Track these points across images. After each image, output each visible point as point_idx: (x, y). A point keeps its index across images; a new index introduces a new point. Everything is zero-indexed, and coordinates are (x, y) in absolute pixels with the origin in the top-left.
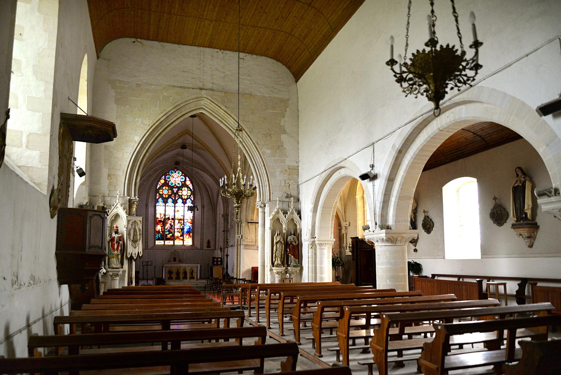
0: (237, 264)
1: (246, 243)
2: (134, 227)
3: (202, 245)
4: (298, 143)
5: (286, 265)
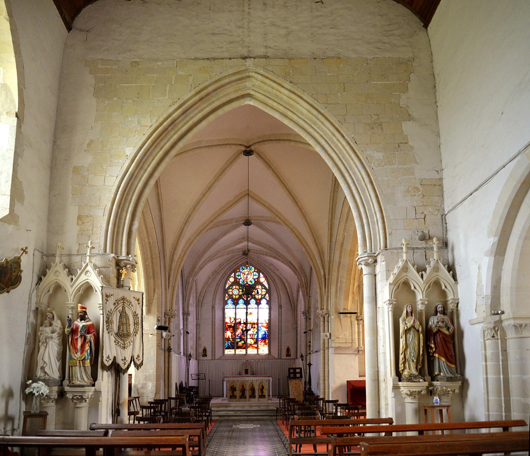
0: (324, 376)
1: (337, 345)
2: (121, 308)
3: (280, 353)
4: (438, 135)
5: (428, 378)
